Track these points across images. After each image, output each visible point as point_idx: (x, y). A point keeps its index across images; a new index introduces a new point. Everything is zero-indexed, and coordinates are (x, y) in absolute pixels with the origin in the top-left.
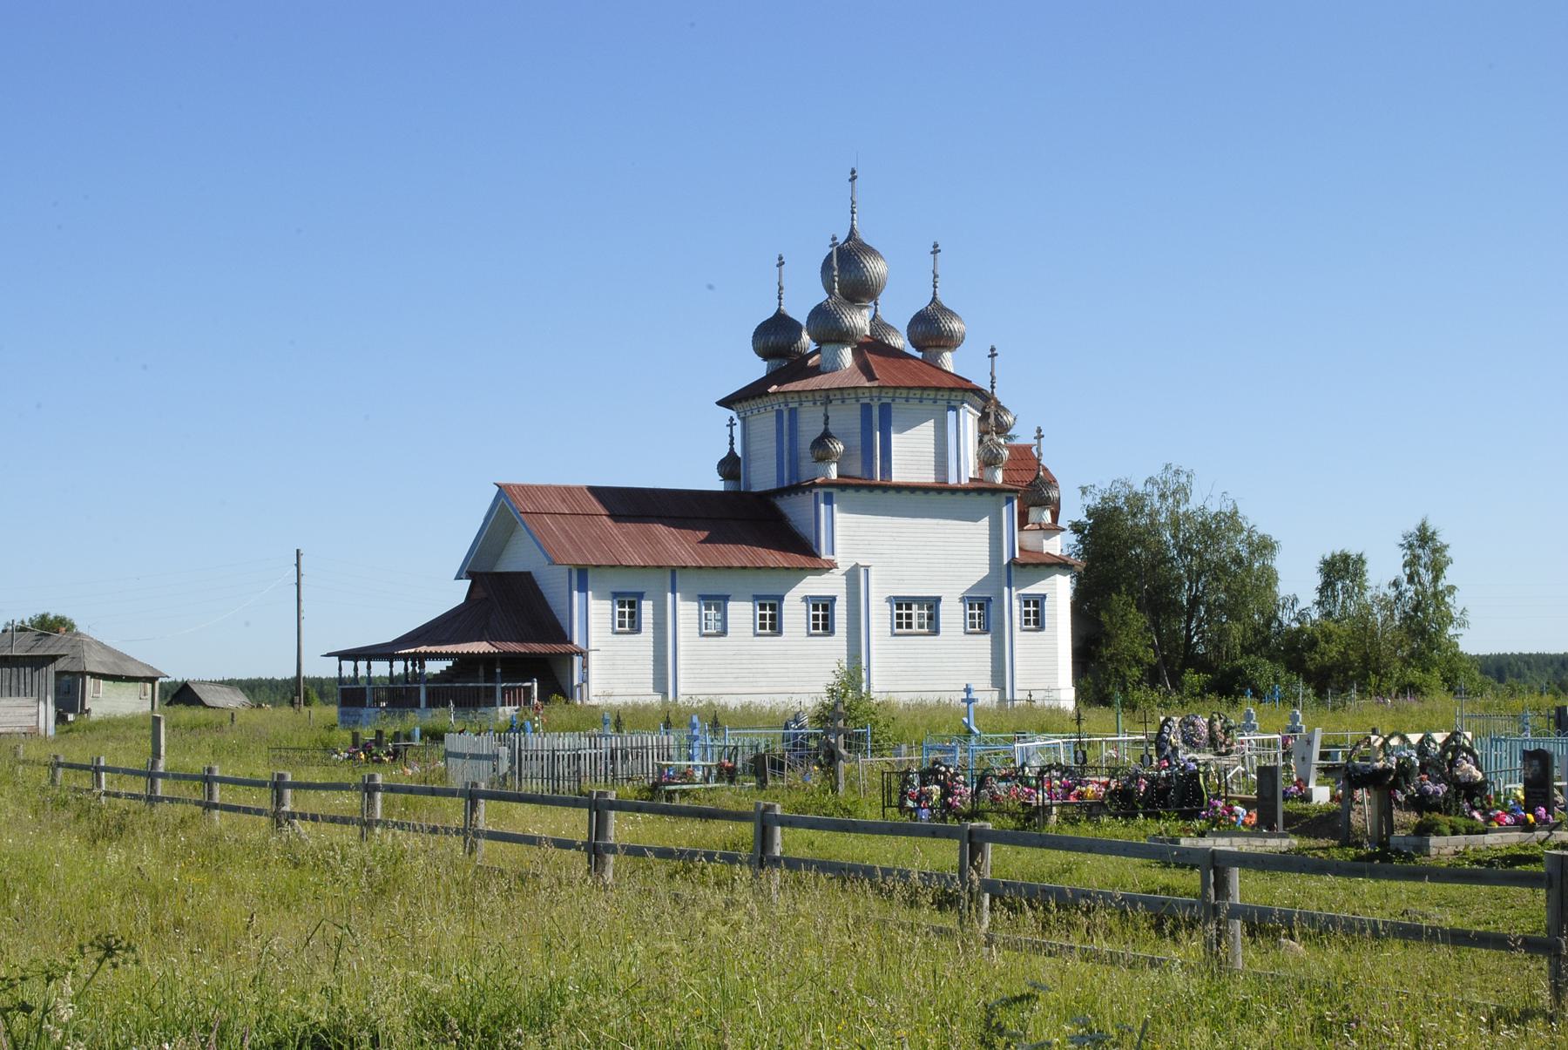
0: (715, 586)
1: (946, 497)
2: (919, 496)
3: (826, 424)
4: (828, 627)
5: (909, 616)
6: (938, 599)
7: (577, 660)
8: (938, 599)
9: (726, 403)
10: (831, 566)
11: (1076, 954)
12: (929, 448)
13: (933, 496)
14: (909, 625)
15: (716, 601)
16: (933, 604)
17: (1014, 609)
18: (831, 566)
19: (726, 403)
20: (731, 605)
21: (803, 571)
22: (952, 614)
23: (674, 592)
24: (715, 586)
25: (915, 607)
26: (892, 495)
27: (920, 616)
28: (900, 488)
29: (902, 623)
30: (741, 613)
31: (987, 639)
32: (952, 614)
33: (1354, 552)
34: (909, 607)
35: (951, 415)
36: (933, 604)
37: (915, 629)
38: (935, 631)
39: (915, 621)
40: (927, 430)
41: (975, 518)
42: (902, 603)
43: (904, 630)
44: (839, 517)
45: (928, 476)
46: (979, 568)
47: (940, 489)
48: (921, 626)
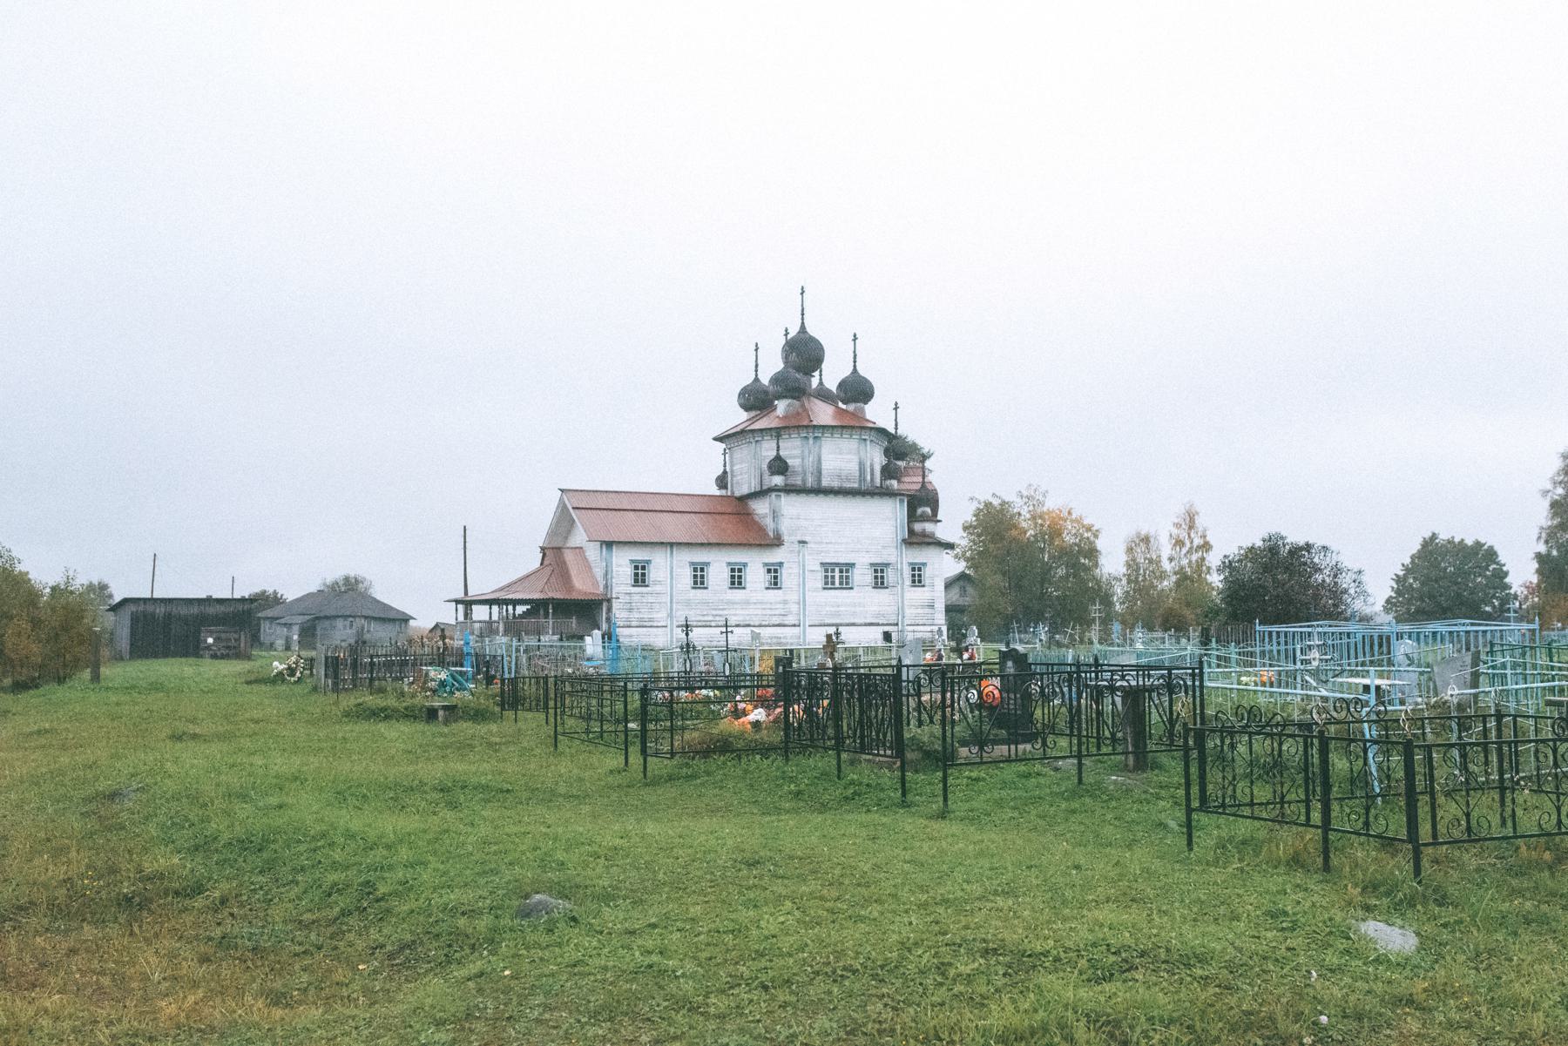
7: (605, 605)
8: (853, 565)
9: (719, 439)
19: (719, 439)
22: (863, 576)
29: (829, 584)
32: (863, 576)
42: (828, 567)
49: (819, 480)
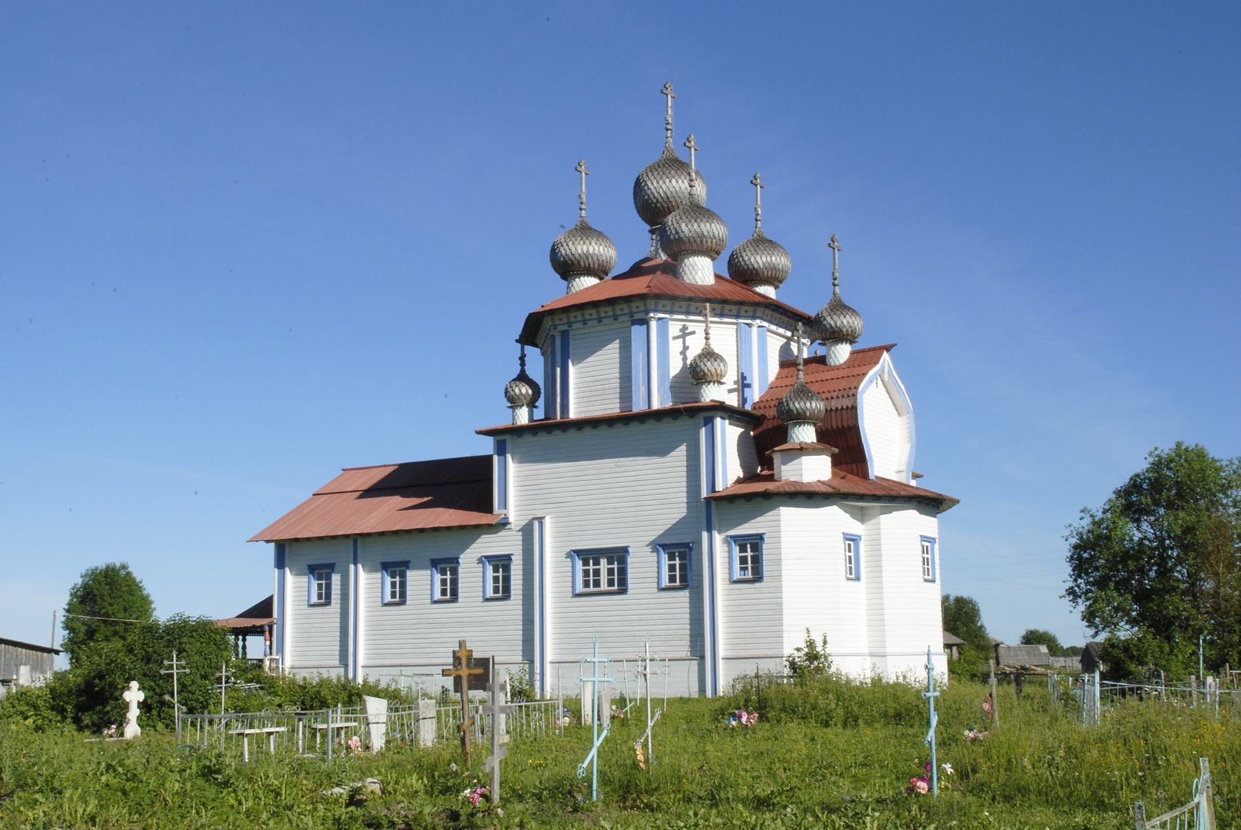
0: (395, 552)
1: (634, 427)
2: (604, 431)
3: (523, 364)
4: (504, 592)
5: (597, 573)
6: (625, 550)
8: (625, 550)
10: (504, 524)
11: (993, 680)
12: (615, 373)
13: (619, 429)
14: (597, 583)
15: (396, 568)
16: (619, 555)
17: (719, 552)
18: (504, 524)
20: (410, 574)
21: (479, 529)
22: (646, 568)
23: (355, 564)
24: (395, 552)
25: (603, 562)
26: (572, 434)
27: (610, 572)
28: (580, 424)
29: (590, 587)
30: (421, 581)
31: (684, 596)
33: (649, 549)
34: (597, 563)
35: (637, 331)
36: (619, 555)
37: (604, 586)
38: (623, 589)
39: (604, 578)
40: (612, 351)
41: (663, 451)
43: (592, 589)
44: (512, 466)
45: (612, 407)
46: (671, 507)
47: (626, 419)
48: (611, 583)
49: (432, 576)
